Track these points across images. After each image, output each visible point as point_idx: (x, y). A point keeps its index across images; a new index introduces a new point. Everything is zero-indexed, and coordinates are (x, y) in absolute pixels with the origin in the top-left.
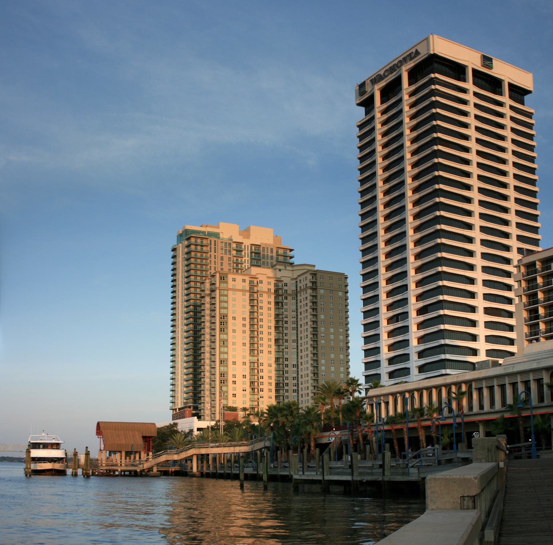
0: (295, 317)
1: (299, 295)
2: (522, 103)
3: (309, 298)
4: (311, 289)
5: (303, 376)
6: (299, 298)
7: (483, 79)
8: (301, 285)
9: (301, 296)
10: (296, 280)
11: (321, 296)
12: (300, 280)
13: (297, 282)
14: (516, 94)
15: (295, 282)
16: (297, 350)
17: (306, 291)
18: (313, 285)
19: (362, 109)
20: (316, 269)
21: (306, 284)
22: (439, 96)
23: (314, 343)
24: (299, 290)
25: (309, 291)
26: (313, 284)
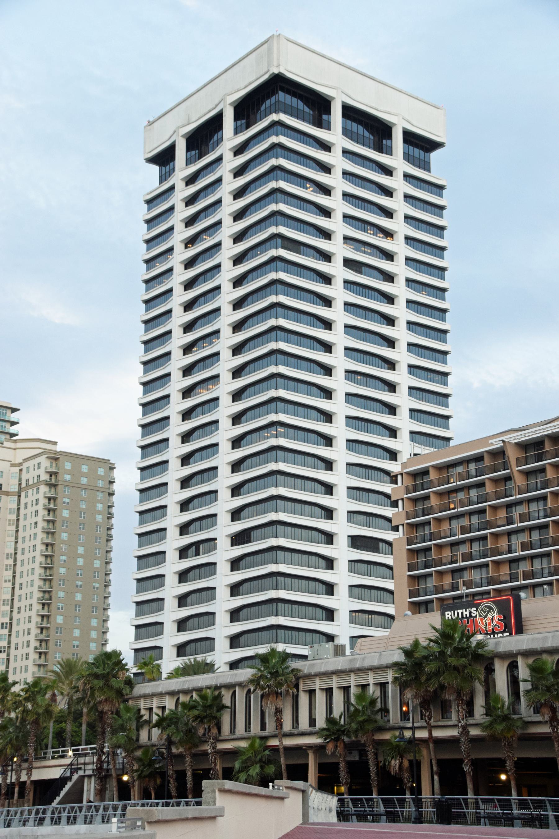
0: (9, 581)
1: (23, 494)
2: (426, 167)
3: (43, 501)
4: (46, 484)
5: (18, 670)
6: (23, 500)
7: (360, 122)
8: (29, 476)
9: (26, 496)
10: (20, 468)
11: (57, 628)
12: (28, 468)
13: (21, 470)
14: (416, 150)
15: (18, 471)
16: (14, 584)
17: (38, 489)
18: (51, 479)
19: (155, 169)
20: (59, 448)
21: (39, 476)
22: (285, 113)
23: (48, 525)
24: (24, 485)
25: (44, 489)
26: (51, 476)
